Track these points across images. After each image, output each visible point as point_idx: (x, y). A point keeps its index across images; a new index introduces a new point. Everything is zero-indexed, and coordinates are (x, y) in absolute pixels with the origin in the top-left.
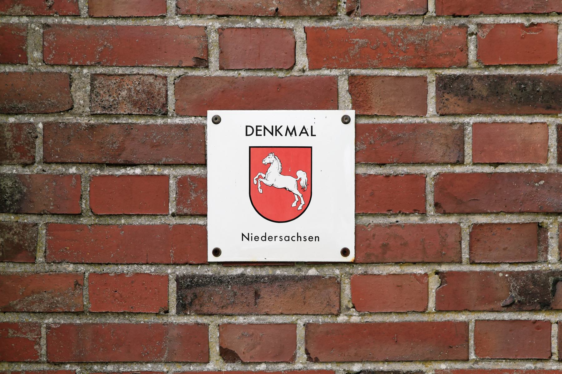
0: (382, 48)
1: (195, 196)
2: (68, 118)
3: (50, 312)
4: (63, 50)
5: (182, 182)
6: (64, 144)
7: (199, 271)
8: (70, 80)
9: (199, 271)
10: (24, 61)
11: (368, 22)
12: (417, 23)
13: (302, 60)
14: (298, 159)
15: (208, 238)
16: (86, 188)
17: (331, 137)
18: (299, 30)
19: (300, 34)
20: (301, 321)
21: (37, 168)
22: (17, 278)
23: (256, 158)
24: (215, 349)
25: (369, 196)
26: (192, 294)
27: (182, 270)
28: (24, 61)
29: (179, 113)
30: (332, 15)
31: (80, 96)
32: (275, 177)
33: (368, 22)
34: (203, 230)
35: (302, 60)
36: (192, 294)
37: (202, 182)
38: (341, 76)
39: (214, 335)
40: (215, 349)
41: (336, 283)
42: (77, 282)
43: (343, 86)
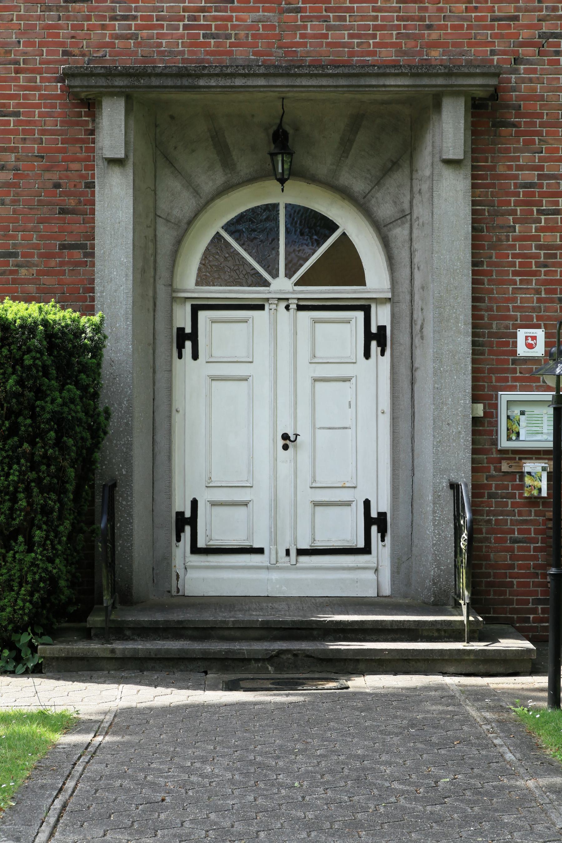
0: (549, 318)
1: (515, 344)
2: (492, 330)
3: (488, 365)
4: (492, 318)
5: (513, 342)
6: (491, 335)
7: (515, 357)
8: (492, 323)
9: (515, 357)
10: (484, 320)
11: (547, 314)
12: (556, 314)
13: (535, 320)
14: (534, 338)
15: (426, 648)
16: (495, 343)
17: (540, 334)
18: (534, 315)
19: (535, 316)
20: (534, 367)
21: (486, 339)
22: (482, 359)
23: (527, 338)
24: (518, 372)
25: (547, 344)
26: (514, 362)
27: (512, 357)
28: (484, 320)
29: (512, 329)
30: (541, 312)
31: (494, 326)
32: (530, 341)
33: (547, 314)
34: (516, 351)
35: (535, 320)
36: (514, 362)
37: (516, 342)
38: (542, 323)
39: (518, 369)
40: (518, 372)
41: (541, 360)
42: (493, 359)
43: (542, 325)
